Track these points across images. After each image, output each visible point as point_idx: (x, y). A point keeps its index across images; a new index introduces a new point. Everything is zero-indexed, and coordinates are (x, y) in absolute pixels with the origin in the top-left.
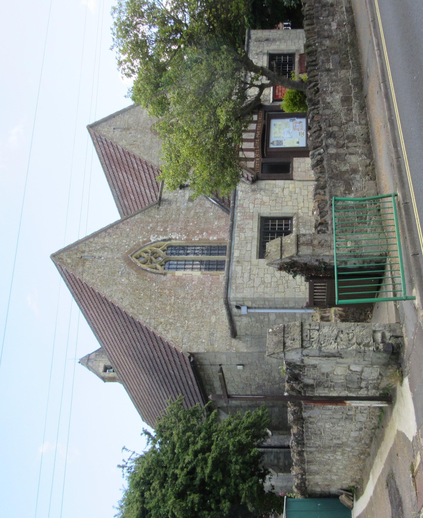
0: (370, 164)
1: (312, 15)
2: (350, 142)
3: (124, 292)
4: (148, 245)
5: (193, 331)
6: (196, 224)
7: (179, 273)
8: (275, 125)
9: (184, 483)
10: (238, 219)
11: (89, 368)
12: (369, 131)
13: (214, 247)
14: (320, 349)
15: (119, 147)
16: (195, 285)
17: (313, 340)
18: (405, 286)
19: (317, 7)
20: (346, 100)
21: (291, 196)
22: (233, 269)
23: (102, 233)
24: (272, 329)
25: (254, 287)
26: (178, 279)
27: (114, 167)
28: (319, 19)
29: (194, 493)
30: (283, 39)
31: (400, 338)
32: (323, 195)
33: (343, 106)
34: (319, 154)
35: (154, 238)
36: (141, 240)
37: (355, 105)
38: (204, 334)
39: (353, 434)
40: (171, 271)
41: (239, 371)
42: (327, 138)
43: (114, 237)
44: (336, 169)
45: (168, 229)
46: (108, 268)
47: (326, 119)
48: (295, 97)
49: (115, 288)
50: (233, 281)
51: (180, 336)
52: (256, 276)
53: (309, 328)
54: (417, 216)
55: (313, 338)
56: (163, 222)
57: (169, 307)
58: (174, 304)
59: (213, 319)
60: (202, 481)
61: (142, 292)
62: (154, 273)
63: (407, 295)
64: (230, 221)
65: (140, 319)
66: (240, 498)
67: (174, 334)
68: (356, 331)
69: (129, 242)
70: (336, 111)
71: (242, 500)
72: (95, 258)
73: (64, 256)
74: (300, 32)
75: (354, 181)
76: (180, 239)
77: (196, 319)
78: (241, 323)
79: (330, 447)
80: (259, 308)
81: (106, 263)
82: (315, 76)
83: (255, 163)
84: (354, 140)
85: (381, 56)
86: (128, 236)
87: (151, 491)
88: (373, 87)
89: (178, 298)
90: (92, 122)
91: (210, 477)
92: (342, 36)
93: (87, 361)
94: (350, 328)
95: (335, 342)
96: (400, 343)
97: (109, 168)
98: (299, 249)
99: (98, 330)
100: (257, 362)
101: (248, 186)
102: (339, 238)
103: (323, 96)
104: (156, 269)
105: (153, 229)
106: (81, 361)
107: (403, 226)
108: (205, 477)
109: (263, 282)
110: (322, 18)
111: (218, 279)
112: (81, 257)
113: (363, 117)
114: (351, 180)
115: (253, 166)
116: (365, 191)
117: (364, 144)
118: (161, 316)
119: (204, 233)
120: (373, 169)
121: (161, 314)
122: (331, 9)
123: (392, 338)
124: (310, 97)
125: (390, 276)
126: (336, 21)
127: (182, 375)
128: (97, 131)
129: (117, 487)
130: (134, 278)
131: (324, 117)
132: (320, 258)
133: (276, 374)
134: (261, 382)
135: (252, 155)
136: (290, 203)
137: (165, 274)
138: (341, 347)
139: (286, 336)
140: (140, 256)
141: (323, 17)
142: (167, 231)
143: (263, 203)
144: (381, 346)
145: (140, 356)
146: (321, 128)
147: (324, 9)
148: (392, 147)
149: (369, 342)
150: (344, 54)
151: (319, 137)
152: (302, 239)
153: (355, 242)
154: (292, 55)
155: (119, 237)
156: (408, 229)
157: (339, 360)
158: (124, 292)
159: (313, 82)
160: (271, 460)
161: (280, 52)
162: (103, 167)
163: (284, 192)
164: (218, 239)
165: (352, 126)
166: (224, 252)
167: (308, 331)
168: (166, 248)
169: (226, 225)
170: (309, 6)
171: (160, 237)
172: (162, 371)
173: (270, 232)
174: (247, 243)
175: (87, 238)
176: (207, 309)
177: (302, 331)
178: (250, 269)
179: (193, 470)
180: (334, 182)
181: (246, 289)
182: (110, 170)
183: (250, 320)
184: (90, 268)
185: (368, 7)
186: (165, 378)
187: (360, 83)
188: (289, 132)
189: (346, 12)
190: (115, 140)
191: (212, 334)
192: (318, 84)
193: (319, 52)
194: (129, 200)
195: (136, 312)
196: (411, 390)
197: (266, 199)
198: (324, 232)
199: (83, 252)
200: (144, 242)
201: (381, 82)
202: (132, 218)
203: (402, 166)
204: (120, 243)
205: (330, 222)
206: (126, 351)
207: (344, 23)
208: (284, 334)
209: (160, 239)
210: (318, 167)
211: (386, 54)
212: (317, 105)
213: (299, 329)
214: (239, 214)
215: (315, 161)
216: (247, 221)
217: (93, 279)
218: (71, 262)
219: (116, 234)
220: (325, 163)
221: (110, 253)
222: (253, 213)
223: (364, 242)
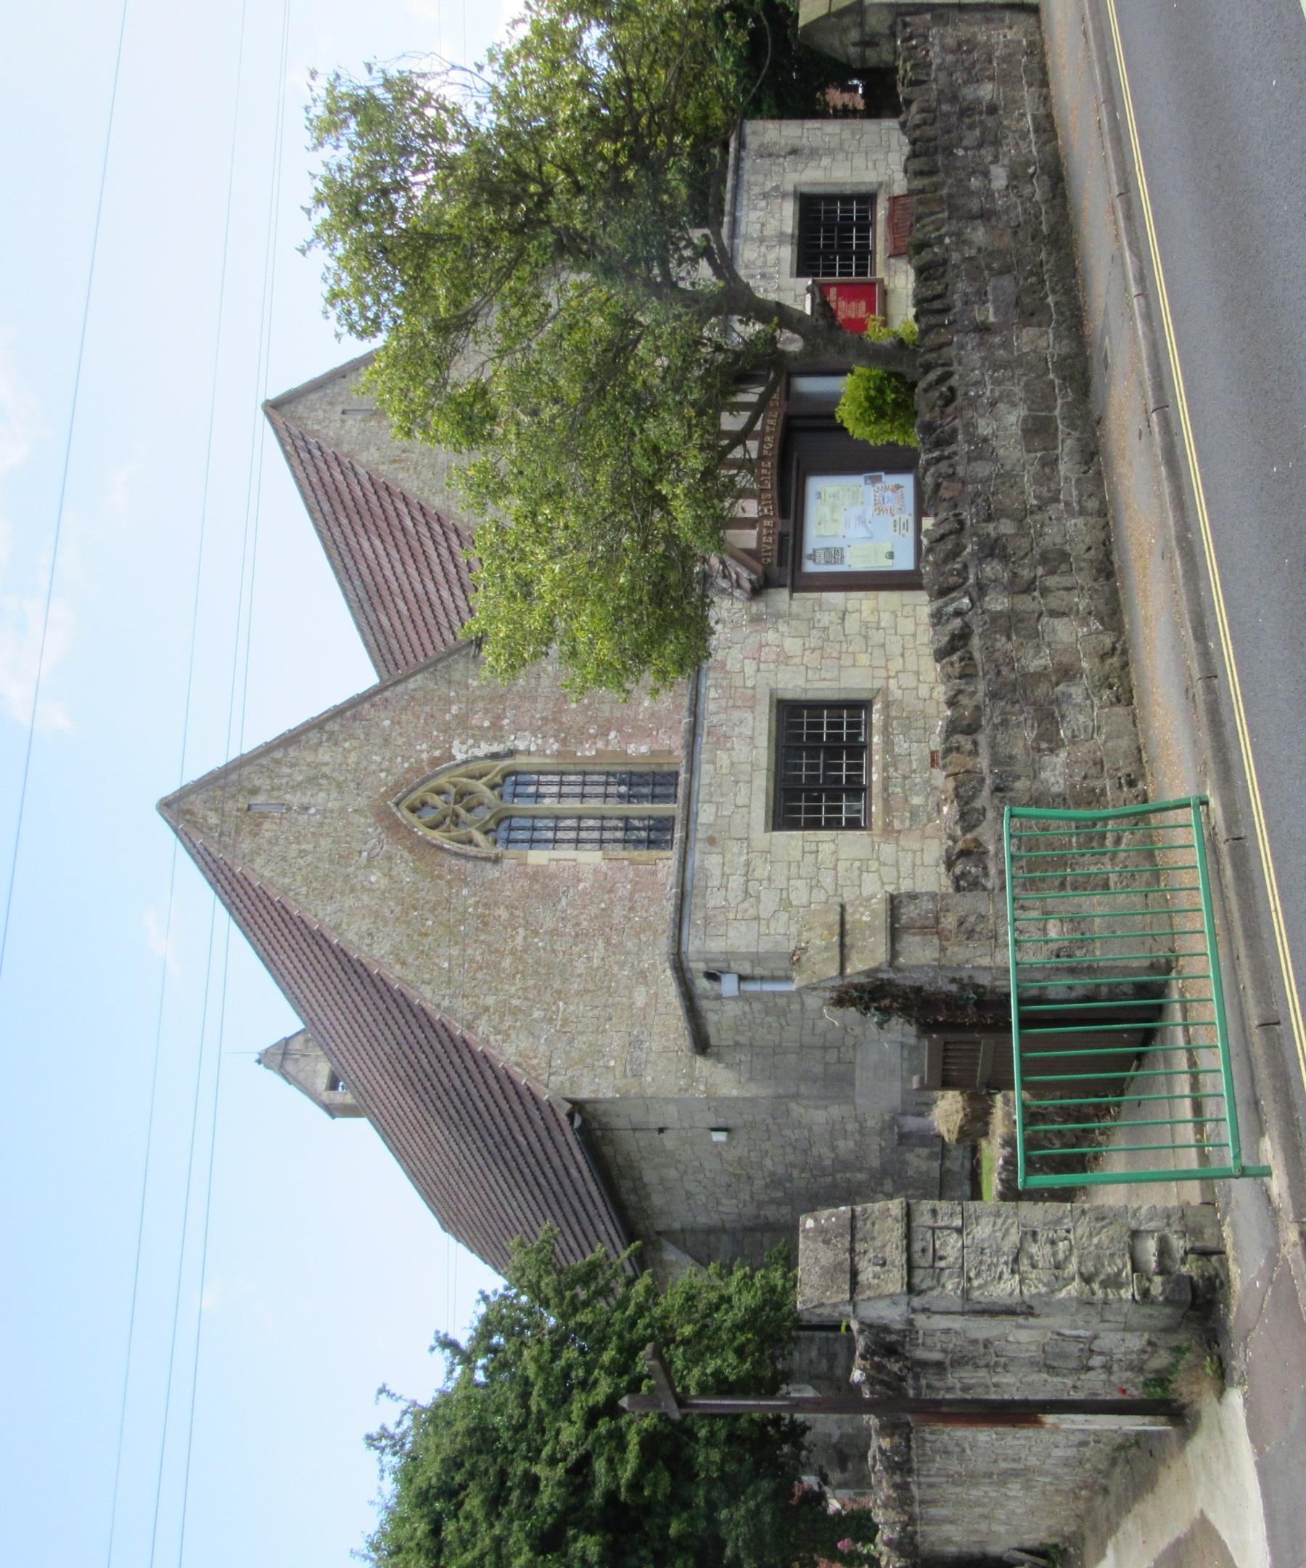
0: (1114, 649)
1: (929, 140)
2: (1052, 572)
3: (377, 914)
4: (449, 769)
5: (582, 1033)
6: (587, 707)
7: (538, 857)
8: (819, 494)
9: (558, 1505)
10: (712, 707)
11: (286, 1076)
12: (1108, 537)
13: (641, 775)
14: (966, 1294)
15: (361, 471)
16: (585, 892)
17: (942, 1264)
18: (1233, 1108)
19: (948, 115)
20: (1038, 430)
21: (866, 637)
22: (697, 864)
23: (310, 735)
24: (816, 1220)
25: (757, 918)
26: (537, 875)
27: (344, 521)
28: (952, 153)
29: (590, 1531)
30: (842, 149)
31: (1214, 1258)
32: (970, 753)
33: (1029, 451)
34: (958, 613)
35: (464, 748)
36: (425, 756)
37: (1066, 446)
38: (615, 1042)
39: (1058, 1453)
40: (513, 851)
41: (716, 1144)
42: (981, 561)
43: (347, 745)
44: (1010, 662)
45: (506, 721)
46: (330, 840)
47: (978, 494)
48: (880, 391)
49: (350, 901)
50: (698, 900)
51: (543, 1048)
52: (765, 883)
53: (930, 1223)
54: (1275, 902)
55: (942, 1258)
56: (491, 700)
58: (525, 950)
59: (640, 997)
60: (611, 1496)
61: (428, 915)
62: (466, 857)
63: (1245, 1161)
64: (685, 712)
65: (427, 996)
66: (721, 1545)
67: (525, 1043)
68: (1080, 1231)
69: (391, 760)
70: (1008, 468)
71: (728, 1552)
72: (289, 809)
73: (197, 803)
74: (889, 129)
75: (1064, 707)
76: (541, 752)
77: (588, 998)
78: (719, 1019)
79: (990, 1475)
80: (774, 979)
81: (321, 824)
82: (941, 346)
83: (760, 536)
84: (1064, 567)
85: (1151, 316)
86: (387, 742)
87: (462, 1522)
88: (1124, 402)
89: (536, 933)
90: (274, 393)
91: (636, 1486)
92: (1025, 211)
93: (280, 1058)
94: (1058, 1221)
95: (1013, 1272)
96: (1217, 1276)
97: (332, 523)
98: (898, 947)
99: (304, 1002)
100: (770, 1121)
101: (738, 605)
102: (1022, 907)
103: (969, 413)
104: (470, 842)
105: (463, 721)
106: (265, 1059)
107: (1226, 913)
108: (618, 1487)
109: (786, 904)
110: (961, 152)
111: (654, 873)
112: (249, 808)
113: (1091, 488)
114: (1057, 701)
115: (752, 544)
116: (1100, 739)
117: (1096, 580)
119: (612, 734)
120: (1125, 665)
121: (485, 982)
122: (990, 121)
123: (1191, 1257)
124: (927, 417)
125: (1184, 1066)
126: (1006, 162)
127: (551, 1151)
128: (293, 418)
129: (361, 1497)
130: (405, 871)
131: (970, 488)
132: (964, 975)
133: (825, 1151)
134: (780, 1170)
135: (751, 508)
136: (863, 659)
137: (496, 860)
138: (1033, 1290)
139: (860, 1247)
140: (424, 804)
141: (966, 149)
142: (501, 728)
143: (783, 659)
144: (1157, 1286)
145: (428, 1084)
146: (961, 523)
147: (967, 120)
148: (1187, 632)
149: (1120, 1272)
150: (1031, 274)
151: (954, 554)
152: (909, 913)
153: (1071, 920)
154: (867, 199)
155: (361, 747)
156: (1245, 930)
157: (1021, 1320)
158: (377, 914)
159: (937, 365)
160: (811, 1361)
161: (832, 190)
162: (314, 520)
163: (847, 624)
164: (653, 753)
165: (1059, 519)
166: (672, 790)
167: (929, 1233)
168: (498, 779)
169: (677, 708)
170: (922, 111)
171: (483, 745)
172: (492, 1128)
173: (806, 748)
174: (737, 782)
175: (268, 748)
176: (622, 965)
177: (908, 1235)
178: (748, 864)
179: (583, 1464)
180: (1003, 713)
181: (736, 924)
182: (336, 531)
183: (747, 1008)
184: (273, 842)
185: (1108, 145)
186: (503, 1148)
187: (1079, 374)
188: (861, 520)
189: (1036, 131)
190: (346, 448)
191: (636, 1043)
192: (949, 375)
193: (955, 266)
194: (393, 613)
195: (411, 977)
196: (1253, 1439)
197: (793, 646)
198: (975, 885)
199: (254, 791)
200: (434, 762)
201: (1151, 407)
202: (400, 688)
203: (1224, 710)
204: (364, 764)
205: (991, 848)
206: (389, 1067)
207: (1031, 170)
208: (852, 1241)
209: (480, 753)
210: (955, 658)
211: (1167, 320)
212: (950, 444)
213: (899, 1229)
214: (712, 694)
215: (946, 639)
217: (284, 874)
218: (218, 817)
219: (352, 736)
220: (976, 642)
221: (334, 795)
223: (1098, 920)
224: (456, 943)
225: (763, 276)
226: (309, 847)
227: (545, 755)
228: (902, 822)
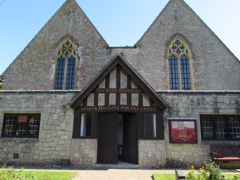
5: (15, 79)
26: (50, 66)
43: (83, 27)
57: (32, 64)
72: (69, 19)
76: (79, 64)
105: (88, 47)
118: (27, 60)
130: (53, 42)
143: (51, 114)
184: (62, 18)
197: (55, 116)
199: (73, 12)
216: (35, 103)
224: (37, 54)
227: (78, 65)
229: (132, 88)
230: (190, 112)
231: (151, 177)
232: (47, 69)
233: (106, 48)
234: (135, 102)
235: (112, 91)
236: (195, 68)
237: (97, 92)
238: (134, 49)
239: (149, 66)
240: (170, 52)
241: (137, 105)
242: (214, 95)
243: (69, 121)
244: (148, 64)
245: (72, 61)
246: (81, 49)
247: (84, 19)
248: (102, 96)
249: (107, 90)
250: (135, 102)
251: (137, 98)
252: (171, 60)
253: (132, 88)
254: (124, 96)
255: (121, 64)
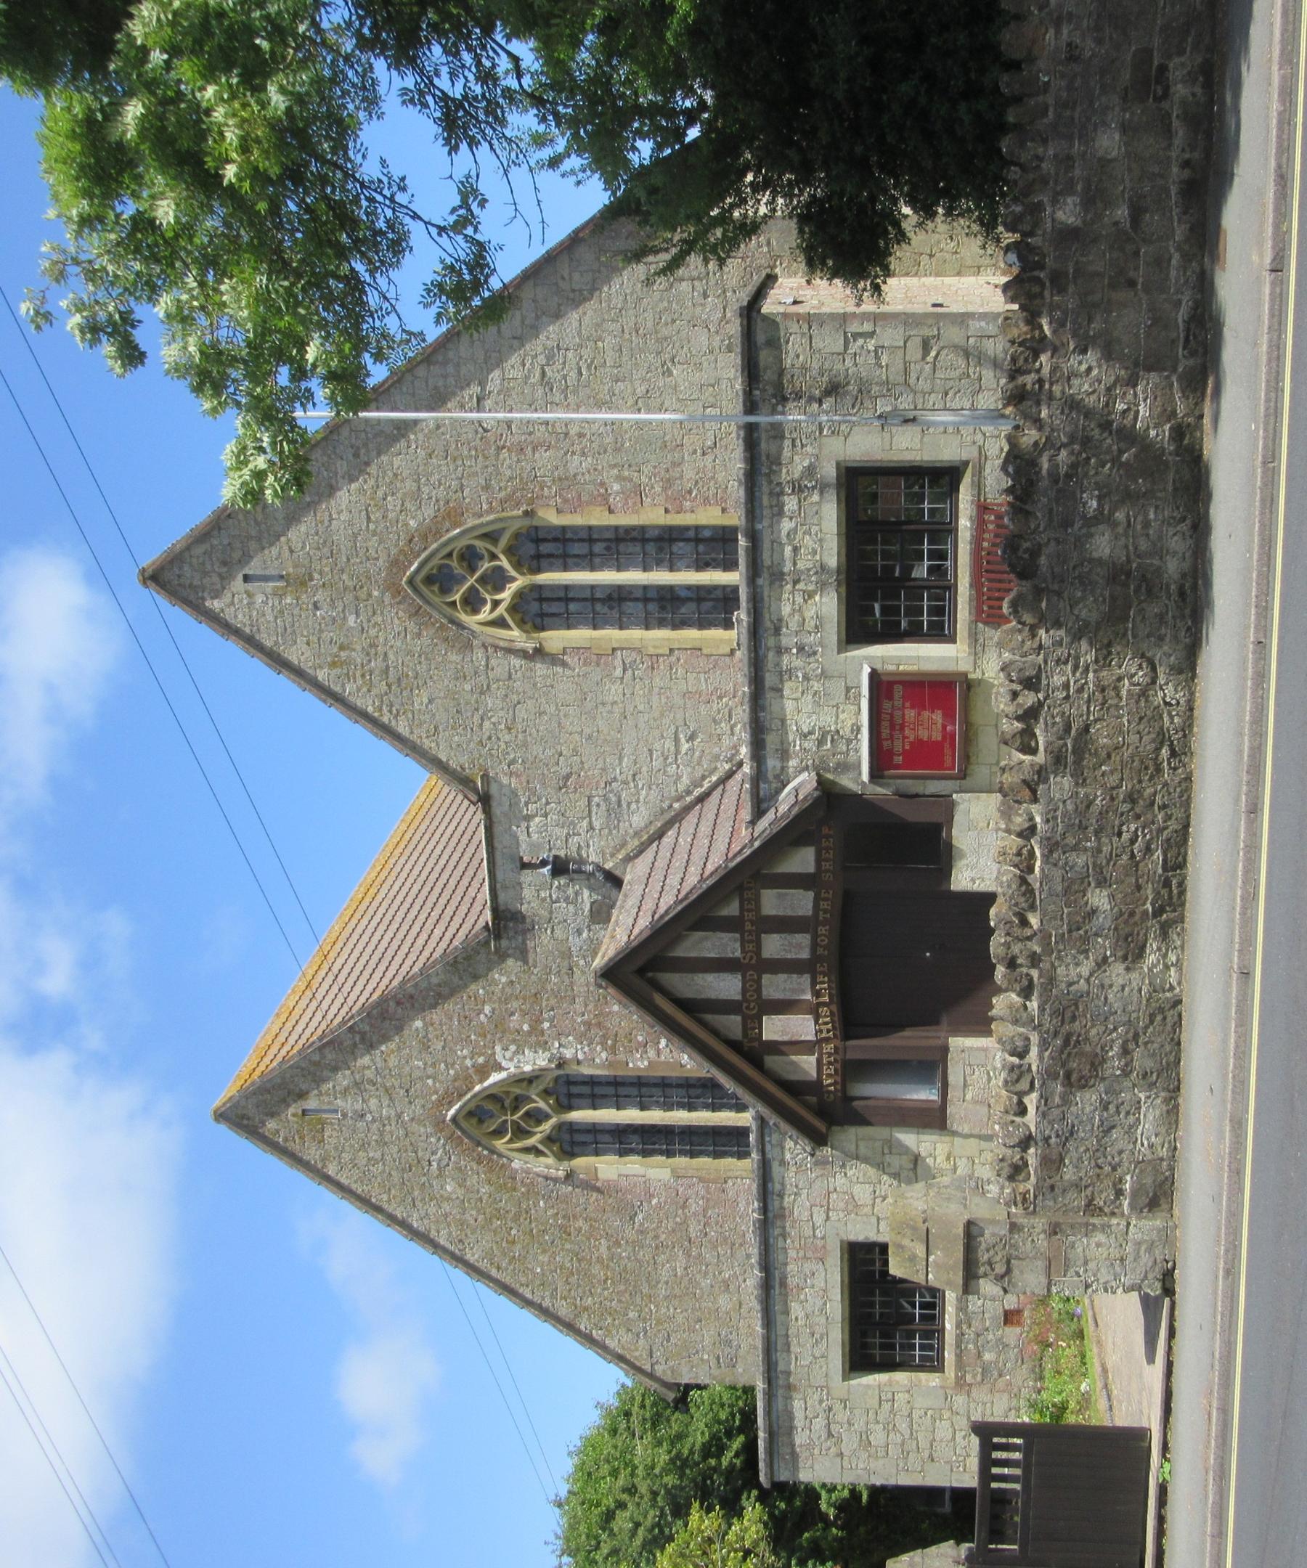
22: (780, 1407)
36: (468, 1063)
72: (344, 1115)
89: (617, 1244)
135: (801, 1026)
142: (542, 1032)
143: (853, 1206)
222: (823, 1238)
225: (801, 649)
226: (378, 1155)
228: (974, 1376)
229: (737, 913)
230: (837, 688)
231: (223, 1130)
232: (622, 1201)
233: (498, 937)
234: (802, 903)
235: (752, 987)
236: (589, 503)
237: (756, 1044)
238: (494, 804)
239: (587, 731)
240: (500, 623)
241: (811, 894)
242: (760, 581)
243: (878, 1144)
244: (577, 737)
245: (570, 1088)
246: (508, 1054)
247: (341, 1043)
248: (774, 1028)
249: (748, 1008)
250: (802, 903)
251: (780, 896)
252: (542, 615)
253: (737, 913)
254: (774, 945)
255: (639, 962)
